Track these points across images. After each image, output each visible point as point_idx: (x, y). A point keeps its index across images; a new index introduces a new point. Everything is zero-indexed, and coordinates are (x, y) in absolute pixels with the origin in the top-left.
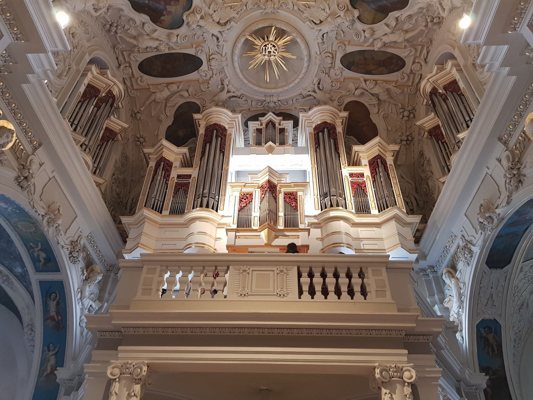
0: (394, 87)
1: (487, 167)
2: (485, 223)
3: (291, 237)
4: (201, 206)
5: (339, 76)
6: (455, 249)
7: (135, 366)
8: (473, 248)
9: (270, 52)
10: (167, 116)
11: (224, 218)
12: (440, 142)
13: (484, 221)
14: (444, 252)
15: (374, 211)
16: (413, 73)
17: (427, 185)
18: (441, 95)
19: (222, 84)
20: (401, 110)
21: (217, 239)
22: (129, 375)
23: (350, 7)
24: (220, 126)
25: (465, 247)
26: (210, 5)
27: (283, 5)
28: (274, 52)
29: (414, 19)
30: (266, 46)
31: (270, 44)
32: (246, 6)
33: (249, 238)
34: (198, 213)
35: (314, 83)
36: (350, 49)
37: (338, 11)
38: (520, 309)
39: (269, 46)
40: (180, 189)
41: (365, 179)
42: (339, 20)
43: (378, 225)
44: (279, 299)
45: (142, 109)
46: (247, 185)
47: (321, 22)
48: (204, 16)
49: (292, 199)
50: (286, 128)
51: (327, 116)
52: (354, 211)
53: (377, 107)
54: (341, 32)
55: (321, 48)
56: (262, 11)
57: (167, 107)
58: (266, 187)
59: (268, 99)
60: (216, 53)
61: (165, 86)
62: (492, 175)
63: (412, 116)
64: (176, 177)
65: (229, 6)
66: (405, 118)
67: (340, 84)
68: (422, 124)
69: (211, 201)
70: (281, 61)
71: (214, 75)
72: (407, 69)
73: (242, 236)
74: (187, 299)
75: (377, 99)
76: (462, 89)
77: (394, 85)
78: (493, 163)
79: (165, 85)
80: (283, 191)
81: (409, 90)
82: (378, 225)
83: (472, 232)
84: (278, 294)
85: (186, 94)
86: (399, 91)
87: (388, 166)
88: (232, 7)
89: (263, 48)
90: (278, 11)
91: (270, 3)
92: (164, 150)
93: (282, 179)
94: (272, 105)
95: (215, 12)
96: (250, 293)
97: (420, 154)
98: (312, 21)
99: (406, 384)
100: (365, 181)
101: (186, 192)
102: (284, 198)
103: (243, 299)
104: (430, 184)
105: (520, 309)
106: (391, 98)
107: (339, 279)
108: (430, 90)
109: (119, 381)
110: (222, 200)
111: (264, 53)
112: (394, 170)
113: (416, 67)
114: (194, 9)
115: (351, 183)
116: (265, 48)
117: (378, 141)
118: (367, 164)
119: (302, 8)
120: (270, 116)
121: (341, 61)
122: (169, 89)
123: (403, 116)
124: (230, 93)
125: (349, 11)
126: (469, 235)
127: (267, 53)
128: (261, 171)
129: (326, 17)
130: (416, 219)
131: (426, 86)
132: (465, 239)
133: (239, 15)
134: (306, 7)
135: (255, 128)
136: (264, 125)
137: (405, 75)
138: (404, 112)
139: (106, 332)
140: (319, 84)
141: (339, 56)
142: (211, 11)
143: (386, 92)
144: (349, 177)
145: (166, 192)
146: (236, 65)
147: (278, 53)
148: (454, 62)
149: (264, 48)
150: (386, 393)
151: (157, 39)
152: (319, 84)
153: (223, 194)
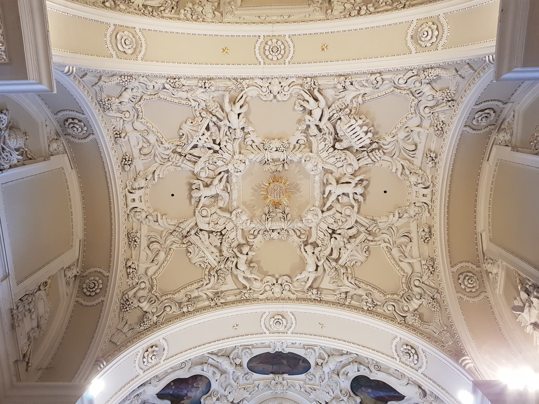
23: (352, 394)
26: (226, 388)
27: (291, 387)
32: (258, 387)
37: (342, 397)
48: (220, 397)
56: (272, 391)
65: (243, 388)
88: (245, 389)
90: (287, 391)
91: (280, 386)
95: (230, 393)
114: (211, 393)
119: (309, 390)
125: (351, 397)
128: (79, 258)
133: (251, 395)
134: (312, 389)
142: (226, 393)
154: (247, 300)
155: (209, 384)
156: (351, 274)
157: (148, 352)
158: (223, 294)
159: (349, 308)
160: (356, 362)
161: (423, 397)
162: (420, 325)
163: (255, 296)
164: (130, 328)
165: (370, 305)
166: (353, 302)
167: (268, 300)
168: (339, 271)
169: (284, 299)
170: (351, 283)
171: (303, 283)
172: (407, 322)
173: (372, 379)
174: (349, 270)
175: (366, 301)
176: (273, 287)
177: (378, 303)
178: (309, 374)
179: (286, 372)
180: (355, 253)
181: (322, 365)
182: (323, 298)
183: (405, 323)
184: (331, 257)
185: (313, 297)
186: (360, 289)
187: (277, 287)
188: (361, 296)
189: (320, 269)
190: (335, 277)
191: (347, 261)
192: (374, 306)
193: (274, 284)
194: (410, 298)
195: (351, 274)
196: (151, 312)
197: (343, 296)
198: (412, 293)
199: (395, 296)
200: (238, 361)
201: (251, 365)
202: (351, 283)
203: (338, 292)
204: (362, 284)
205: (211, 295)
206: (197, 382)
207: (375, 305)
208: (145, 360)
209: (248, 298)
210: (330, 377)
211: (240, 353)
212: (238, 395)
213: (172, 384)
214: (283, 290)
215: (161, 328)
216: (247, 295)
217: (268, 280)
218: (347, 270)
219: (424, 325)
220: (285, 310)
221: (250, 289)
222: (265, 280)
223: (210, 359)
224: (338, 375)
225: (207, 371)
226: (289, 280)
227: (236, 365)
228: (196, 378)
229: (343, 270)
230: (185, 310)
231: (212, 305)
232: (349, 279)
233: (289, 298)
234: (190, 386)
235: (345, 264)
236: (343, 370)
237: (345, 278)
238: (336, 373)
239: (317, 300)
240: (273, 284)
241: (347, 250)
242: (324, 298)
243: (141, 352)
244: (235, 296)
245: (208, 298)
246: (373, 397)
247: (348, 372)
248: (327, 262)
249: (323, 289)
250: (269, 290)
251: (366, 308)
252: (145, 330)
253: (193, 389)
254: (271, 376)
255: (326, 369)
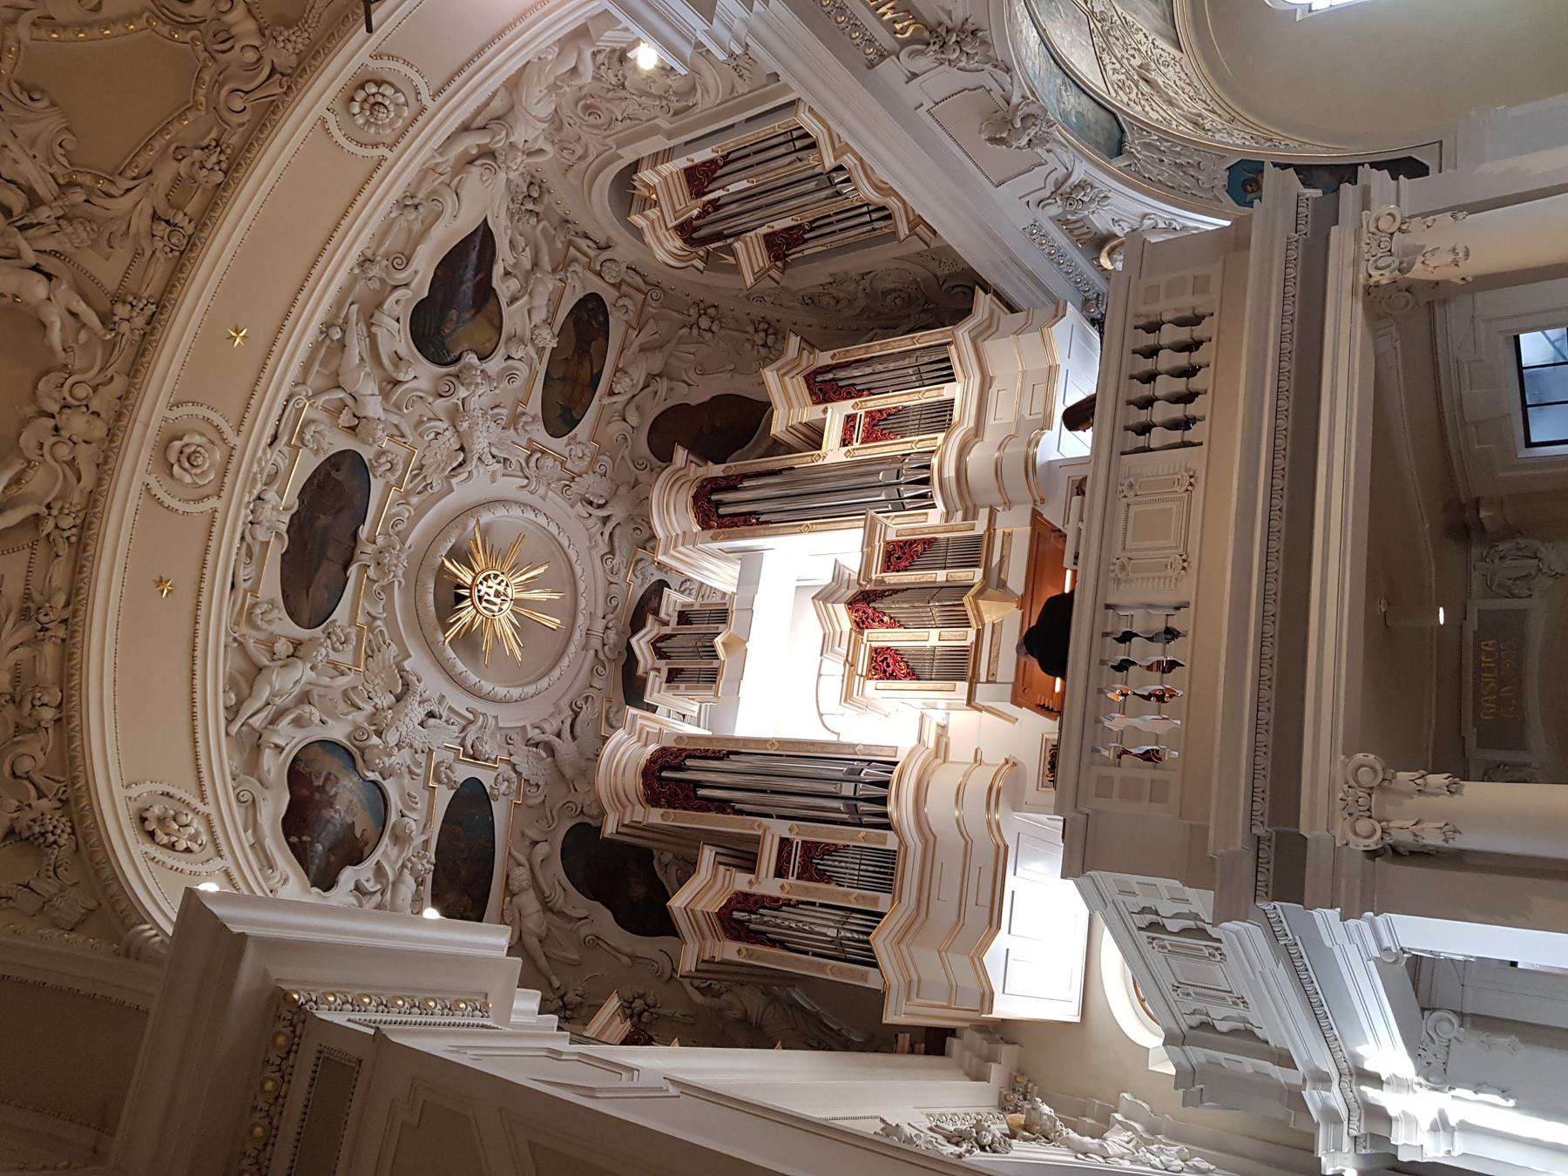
0: (642, 332)
1: (916, 109)
2: (1033, 133)
3: (1004, 552)
4: (883, 801)
5: (586, 451)
6: (1061, 230)
7: (1352, 783)
8: (1074, 179)
9: (497, 594)
10: (586, 918)
11: (925, 737)
12: (806, 236)
13: (1028, 135)
14: (1060, 264)
15: (950, 391)
16: (620, 284)
17: (885, 294)
18: (704, 213)
19: (537, 745)
20: (695, 331)
21: (979, 758)
22: (1373, 796)
24: (653, 760)
25: (1067, 198)
28: (499, 584)
29: (518, 236)
30: (480, 598)
31: (480, 587)
33: (999, 649)
34: (901, 809)
35: (587, 515)
36: (535, 406)
38: (1204, 129)
39: (483, 589)
40: (816, 868)
41: (862, 412)
42: (473, 403)
43: (986, 383)
44: (1200, 487)
45: (556, 983)
46: (850, 659)
47: (462, 449)
49: (904, 553)
50: (678, 608)
51: (678, 491)
52: (941, 436)
53: (675, 384)
54: (496, 411)
55: (514, 473)
56: (396, 584)
57: (566, 910)
58: (864, 612)
59: (596, 643)
60: (462, 735)
61: (511, 901)
62: (937, 101)
63: (712, 311)
64: (780, 881)
65: (366, 659)
66: (714, 328)
67: (604, 454)
68: (754, 273)
69: (869, 773)
70: (521, 575)
71: (513, 759)
72: (608, 295)
73: (991, 667)
74: (1188, 666)
75: (658, 379)
76: (715, 155)
77: (636, 333)
78: (913, 92)
79: (508, 899)
80: (878, 575)
81: (654, 304)
82: (986, 383)
83: (1035, 178)
84: (1187, 490)
85: (542, 849)
86: (651, 327)
87: (835, 362)
89: (485, 608)
92: (698, 908)
93: (846, 576)
94: (612, 636)
96: (1181, 551)
97: (807, 304)
98: (453, 469)
99: (1404, 227)
100: (866, 412)
101: (830, 850)
102: (898, 571)
103: (1195, 564)
104: (888, 284)
105: (1204, 129)
106: (662, 347)
107: (1013, 681)
108: (679, 243)
109: (1388, 821)
110: (867, 752)
111: (496, 608)
112: (848, 351)
113: (611, 275)
114: (354, 746)
115: (868, 442)
116: (486, 601)
117: (775, 372)
118: (822, 407)
120: (641, 644)
121: (555, 435)
122: (523, 890)
123: (710, 330)
124: (563, 731)
125: (460, 375)
126: (1043, 185)
127: (498, 601)
129: (456, 435)
130: (983, 301)
131: (665, 248)
132: (1049, 198)
135: (664, 685)
136: (662, 664)
137: (620, 302)
138: (700, 328)
139: (1258, 857)
140: (591, 503)
141: (540, 434)
143: (649, 354)
144: (849, 448)
145: (822, 905)
146: (501, 691)
147: (503, 573)
148: (645, 164)
149: (484, 604)
150: (1423, 263)
151: (401, 872)
152: (591, 503)
153: (851, 751)
154: (84, 527)
155: (328, 745)
156: (97, 178)
157: (159, 833)
158: (36, 596)
159: (205, 224)
160: (371, 317)
161: (495, 162)
162: (306, 35)
163: (77, 498)
164: (51, 874)
165: (214, 159)
166: (189, 209)
167: (105, 463)
168: (77, 212)
169: (119, 416)
170: (128, 190)
171: (83, 336)
172: (289, 71)
173: (426, 294)
174: (80, 179)
175: (197, 165)
176: (65, 434)
177: (214, 134)
178: (375, 464)
179: (354, 528)
180: (25, 130)
181: (358, 418)
182: (150, 296)
183: (290, 75)
184: (14, 214)
185: (139, 321)
186: (154, 171)
187: (68, 419)
188: (178, 179)
189: (49, 264)
190: (91, 233)
191: (46, 167)
192: (219, 149)
193: (56, 429)
194: (222, 36)
195: (97, 178)
196: (16, 815)
197: (162, 228)
198: (211, 21)
199: (206, 77)
200: (282, 648)
201: (305, 617)
202: (128, 190)
203: (145, 243)
204: (141, 160)
205: (26, 632)
206: (310, 773)
207: (216, 147)
208: (182, 845)
209: (78, 521)
210: (396, 410)
211: (262, 636)
212: (382, 679)
213: (294, 839)
214: (87, 406)
215: (81, 684)
216: (66, 522)
217: (33, 444)
218: (81, 185)
219: (309, 21)
220: (155, 421)
221: (49, 507)
222: (31, 452)
223: (250, 721)
224: (397, 383)
225: (289, 738)
226: (56, 377)
227: (293, 655)
228: (297, 775)
229: (78, 197)
230: (48, 714)
231: (62, 632)
232: (112, 190)
233: (120, 398)
234: (317, 796)
235: (58, 184)
236: (386, 362)
237: (107, 202)
238: (390, 386)
239: (154, 313)
240: (54, 433)
241: (6, 150)
242: (152, 289)
243: (154, 851)
244: (59, 559)
245: (35, 642)
246: (474, 316)
247: (396, 352)
248: (30, 233)
249: (121, 285)
250: (72, 450)
251: (219, 177)
252: (73, 832)
253: (327, 788)
254: (353, 571)
255: (374, 407)
